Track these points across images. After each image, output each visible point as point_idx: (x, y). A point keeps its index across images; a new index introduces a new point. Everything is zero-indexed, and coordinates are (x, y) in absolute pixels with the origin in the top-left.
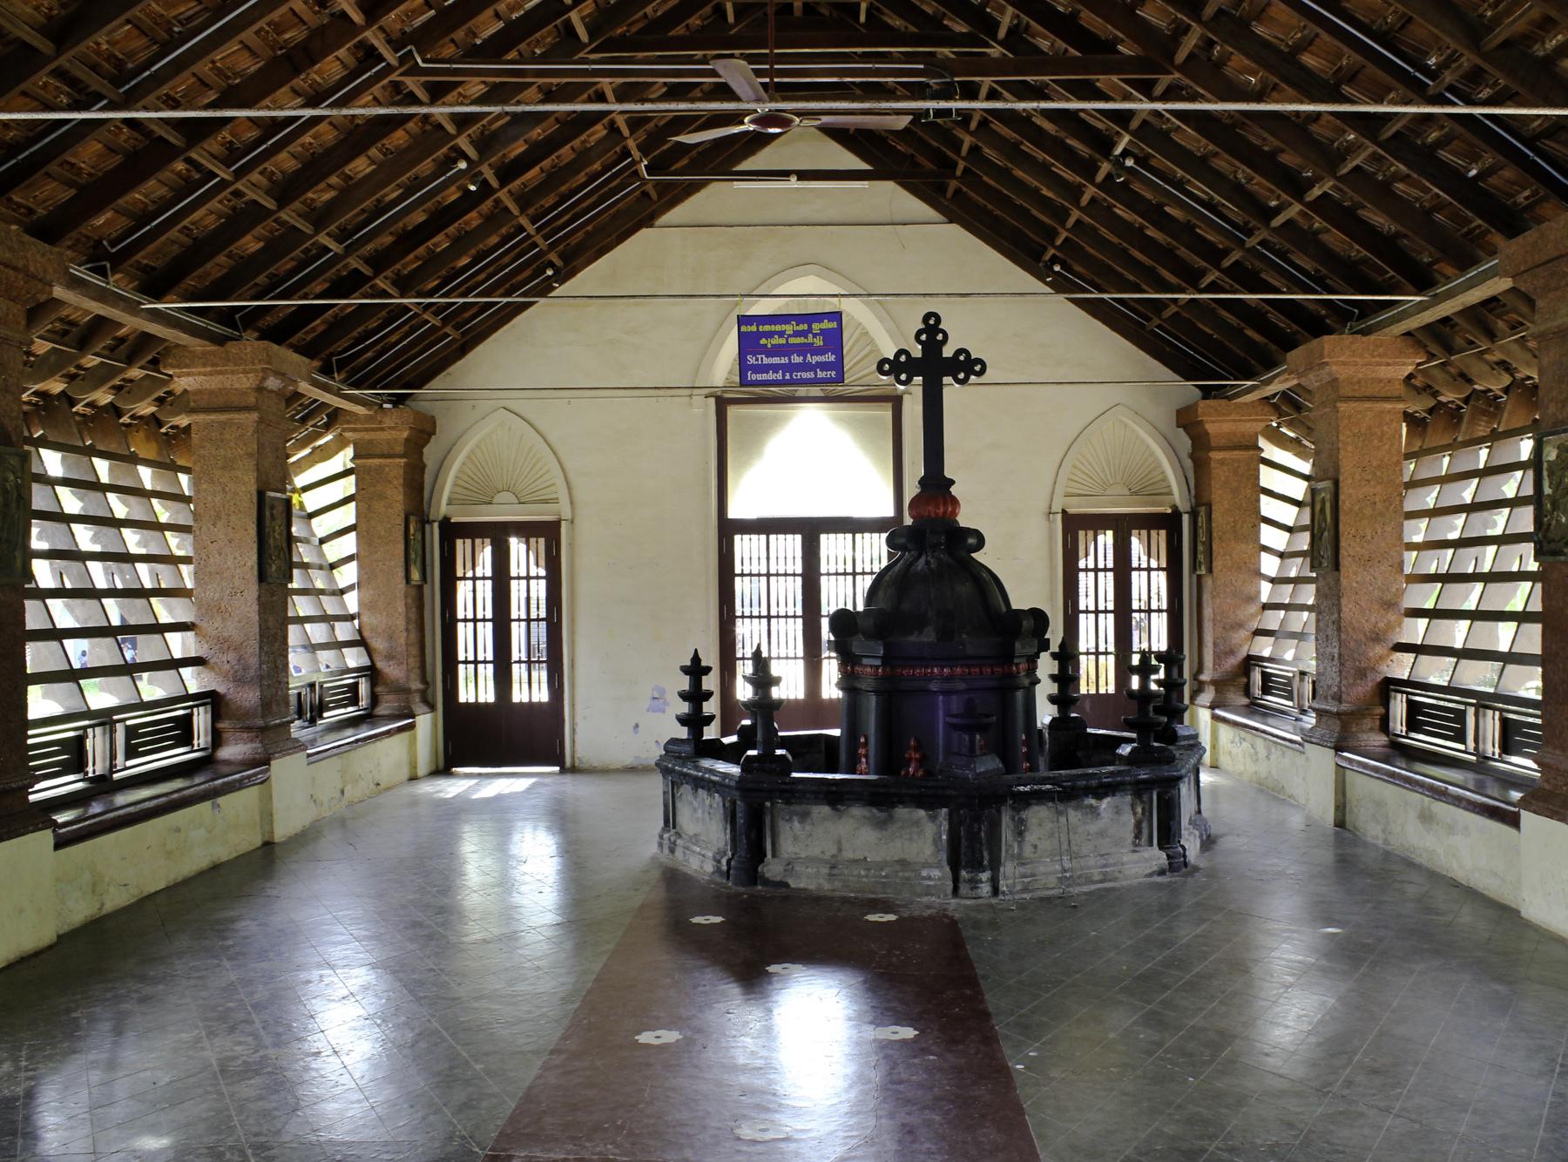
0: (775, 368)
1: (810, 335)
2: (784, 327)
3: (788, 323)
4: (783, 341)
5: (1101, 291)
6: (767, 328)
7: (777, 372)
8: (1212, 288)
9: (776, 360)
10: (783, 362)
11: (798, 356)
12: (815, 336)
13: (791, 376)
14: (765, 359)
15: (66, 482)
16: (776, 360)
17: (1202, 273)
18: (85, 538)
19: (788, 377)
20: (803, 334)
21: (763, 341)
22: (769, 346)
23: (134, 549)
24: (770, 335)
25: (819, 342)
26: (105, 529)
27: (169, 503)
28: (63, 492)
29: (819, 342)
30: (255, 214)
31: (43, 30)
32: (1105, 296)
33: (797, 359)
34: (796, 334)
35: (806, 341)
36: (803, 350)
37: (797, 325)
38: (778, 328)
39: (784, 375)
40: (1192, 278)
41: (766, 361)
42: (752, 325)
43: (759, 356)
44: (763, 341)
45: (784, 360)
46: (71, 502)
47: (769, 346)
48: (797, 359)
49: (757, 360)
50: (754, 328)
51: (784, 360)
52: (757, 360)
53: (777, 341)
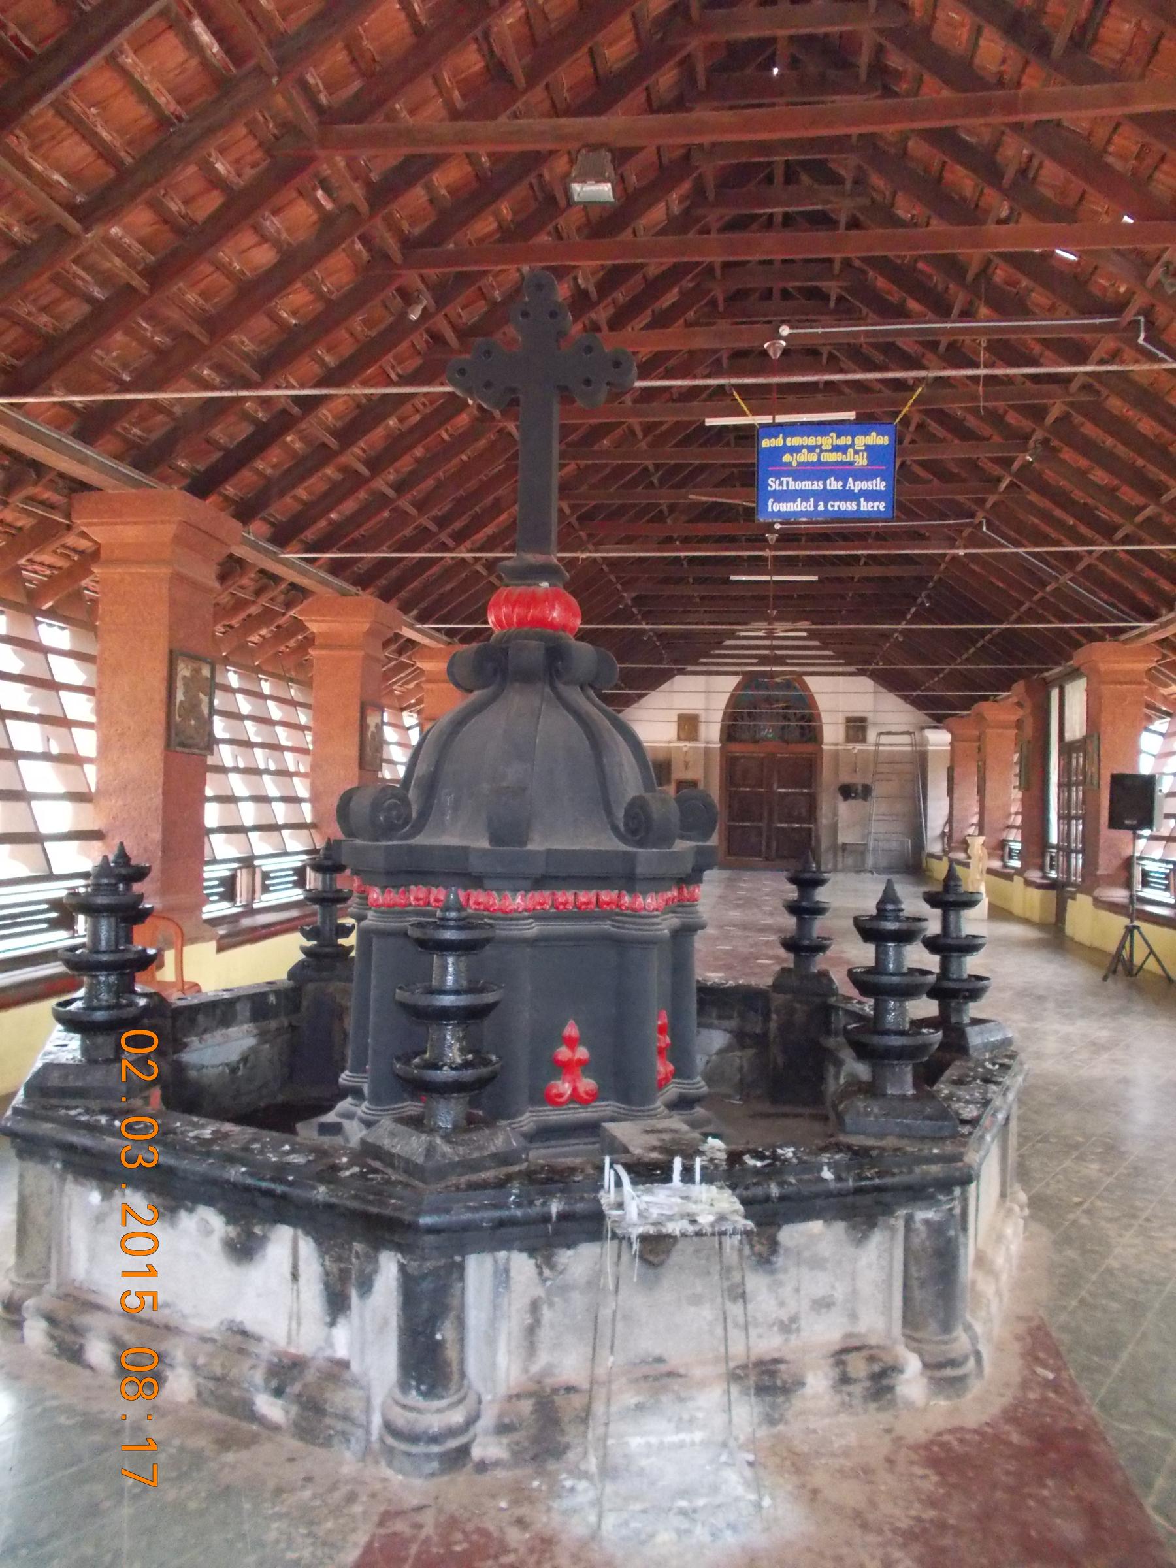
0: (805, 495)
1: (850, 451)
2: (819, 440)
3: (826, 434)
4: (813, 457)
5: (1018, 544)
6: (796, 441)
7: (807, 501)
8: (1126, 540)
9: (806, 485)
10: (815, 487)
11: (837, 480)
12: (856, 452)
13: (826, 506)
14: (792, 483)
15: (272, 698)
16: (806, 485)
17: (1116, 528)
18: (252, 731)
19: (821, 507)
20: (843, 449)
21: (787, 458)
22: (795, 464)
23: (284, 742)
24: (796, 450)
25: (862, 461)
26: (263, 726)
27: (252, 699)
28: (271, 704)
29: (862, 461)
30: (382, 501)
31: (335, 433)
32: (1021, 550)
33: (834, 484)
34: (836, 449)
35: (844, 458)
36: (844, 471)
37: (838, 437)
38: (812, 441)
39: (816, 506)
40: (1108, 532)
41: (794, 485)
42: (776, 437)
43: (784, 479)
44: (787, 458)
45: (817, 486)
46: (245, 705)
47: (795, 464)
48: (834, 484)
49: (781, 484)
50: (779, 442)
51: (817, 486)
52: (781, 484)
53: (805, 457)
